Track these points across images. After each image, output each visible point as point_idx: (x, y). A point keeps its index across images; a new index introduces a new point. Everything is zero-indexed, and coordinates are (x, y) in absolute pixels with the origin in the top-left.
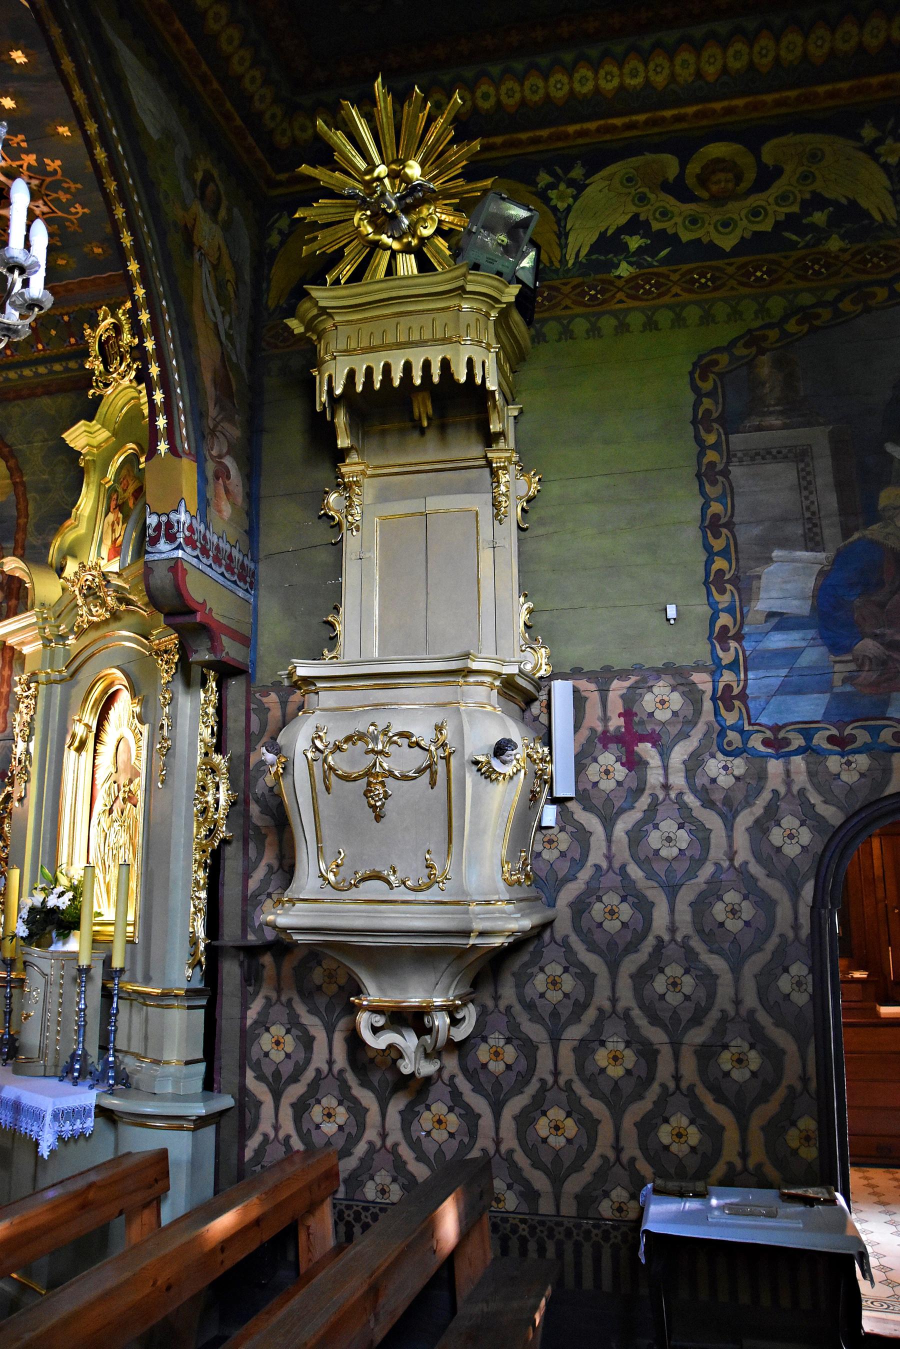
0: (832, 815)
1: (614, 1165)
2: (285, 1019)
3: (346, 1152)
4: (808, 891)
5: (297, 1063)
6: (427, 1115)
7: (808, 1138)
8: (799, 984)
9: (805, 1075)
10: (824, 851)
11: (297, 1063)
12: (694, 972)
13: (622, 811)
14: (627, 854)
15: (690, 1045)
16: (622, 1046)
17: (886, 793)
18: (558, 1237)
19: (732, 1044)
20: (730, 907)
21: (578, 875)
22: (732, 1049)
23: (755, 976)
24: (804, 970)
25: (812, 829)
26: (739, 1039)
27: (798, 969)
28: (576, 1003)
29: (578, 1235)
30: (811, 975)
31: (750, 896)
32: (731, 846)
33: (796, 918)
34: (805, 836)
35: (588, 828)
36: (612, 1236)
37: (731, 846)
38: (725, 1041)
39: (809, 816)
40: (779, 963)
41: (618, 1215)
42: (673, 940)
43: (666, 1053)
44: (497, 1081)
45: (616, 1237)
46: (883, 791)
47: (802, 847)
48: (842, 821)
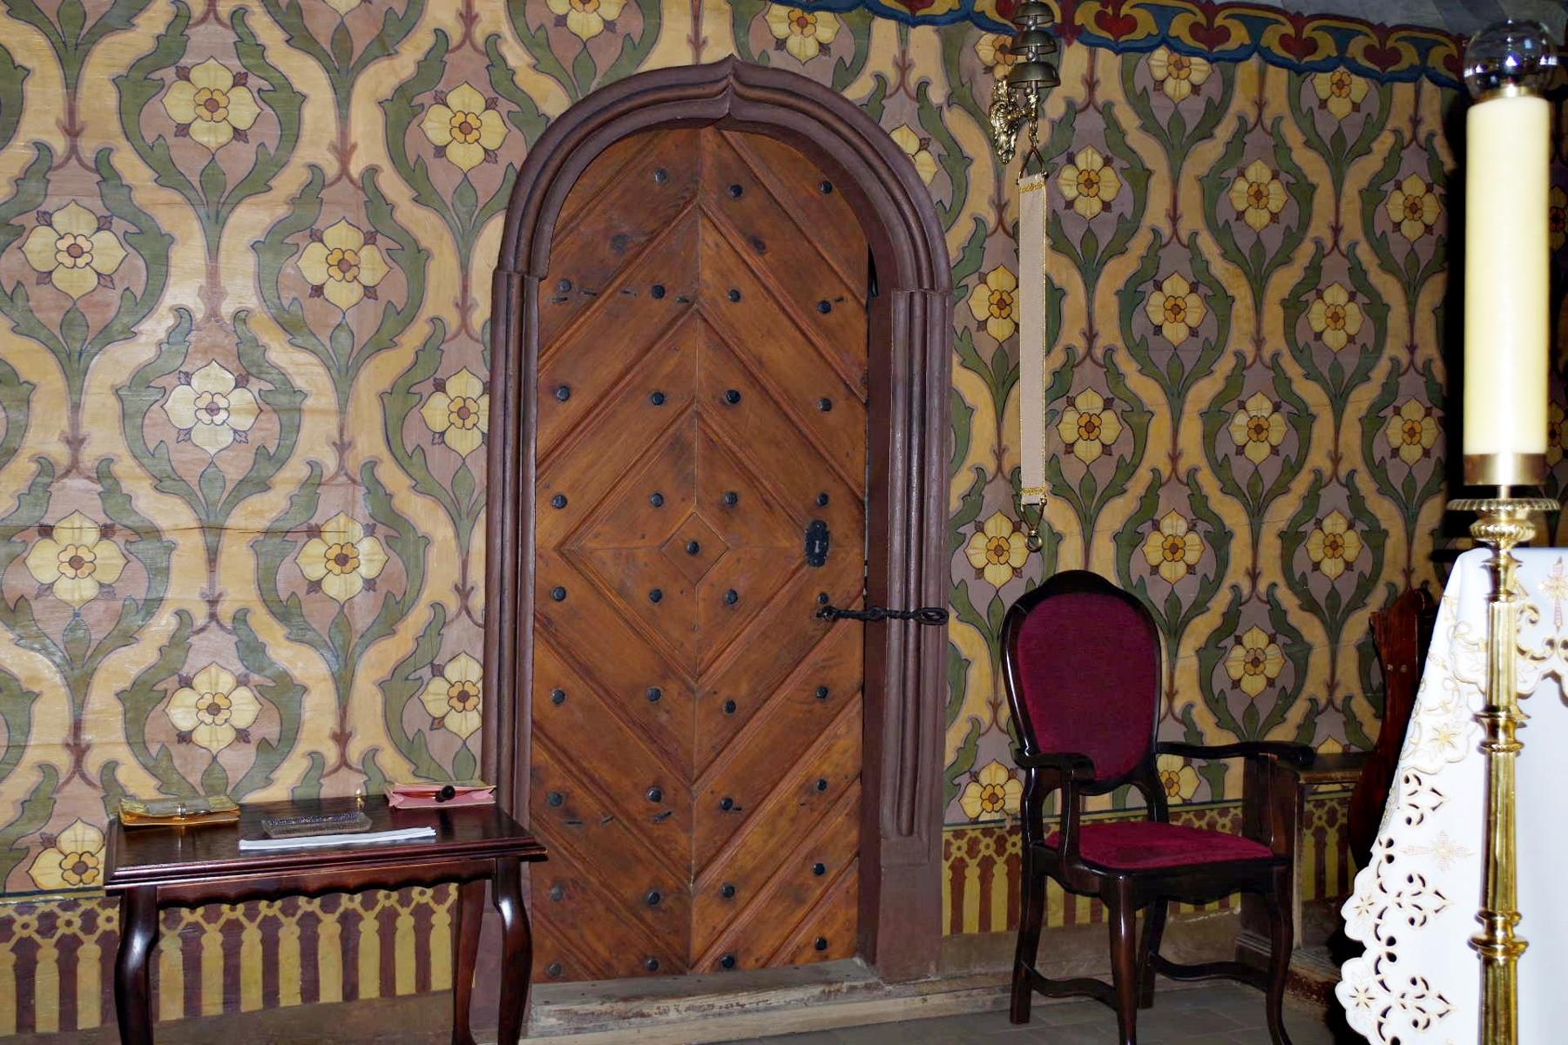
0: (554, 101)
1: (68, 781)
2: (1344, 504)
3: (1278, 716)
4: (492, 234)
5: (1361, 574)
6: (1238, 652)
7: (464, 697)
8: (463, 413)
9: (464, 584)
10: (526, 164)
11: (1361, 574)
12: (255, 385)
13: (104, 28)
14: (115, 126)
15: (245, 531)
16: (92, 536)
17: (645, 68)
18: (984, 852)
19: (328, 527)
20: (337, 256)
21: (273, 183)
22: (327, 536)
23: (381, 396)
24: (475, 388)
25: (510, 118)
26: (342, 519)
27: (467, 385)
28: (261, 452)
29: (987, 846)
30: (486, 399)
31: (379, 237)
32: (344, 134)
33: (465, 288)
34: (493, 128)
35: (298, 86)
36: (60, 922)
37: (344, 134)
38: (313, 522)
39: (500, 86)
40: (425, 377)
41: (77, 878)
42: (213, 314)
43: (190, 547)
44: (343, 614)
45: (69, 923)
46: (640, 62)
47: (486, 150)
48: (563, 110)
